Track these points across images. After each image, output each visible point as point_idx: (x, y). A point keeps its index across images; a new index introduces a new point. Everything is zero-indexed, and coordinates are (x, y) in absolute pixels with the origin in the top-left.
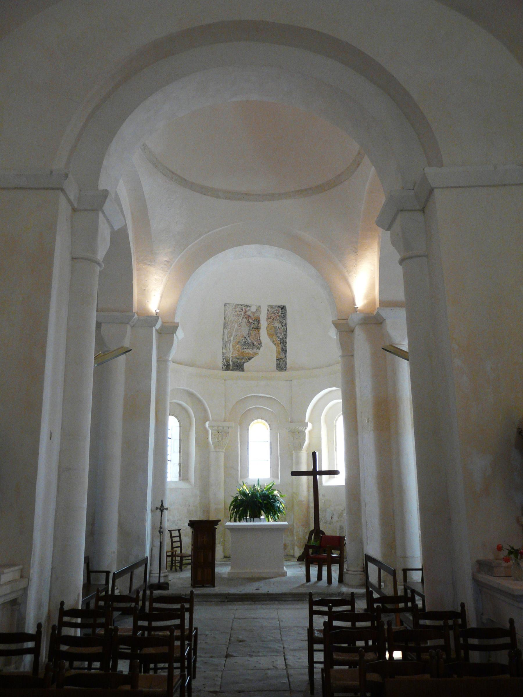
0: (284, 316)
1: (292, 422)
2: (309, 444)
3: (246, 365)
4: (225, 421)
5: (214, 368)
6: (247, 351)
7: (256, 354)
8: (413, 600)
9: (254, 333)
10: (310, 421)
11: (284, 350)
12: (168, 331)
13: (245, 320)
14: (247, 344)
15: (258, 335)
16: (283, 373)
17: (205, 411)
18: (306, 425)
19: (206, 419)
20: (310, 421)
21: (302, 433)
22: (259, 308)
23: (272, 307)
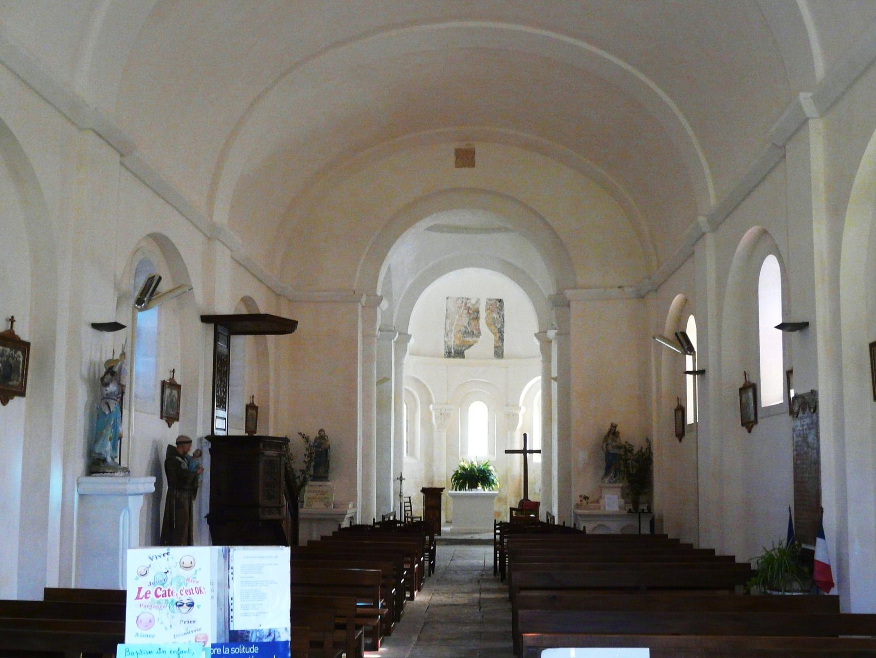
0: (501, 308)
1: (507, 405)
2: (523, 426)
3: (466, 352)
6: (467, 339)
7: (475, 342)
11: (501, 339)
13: (466, 311)
14: (466, 333)
18: (520, 408)
21: (515, 416)
22: (478, 301)
23: (490, 300)
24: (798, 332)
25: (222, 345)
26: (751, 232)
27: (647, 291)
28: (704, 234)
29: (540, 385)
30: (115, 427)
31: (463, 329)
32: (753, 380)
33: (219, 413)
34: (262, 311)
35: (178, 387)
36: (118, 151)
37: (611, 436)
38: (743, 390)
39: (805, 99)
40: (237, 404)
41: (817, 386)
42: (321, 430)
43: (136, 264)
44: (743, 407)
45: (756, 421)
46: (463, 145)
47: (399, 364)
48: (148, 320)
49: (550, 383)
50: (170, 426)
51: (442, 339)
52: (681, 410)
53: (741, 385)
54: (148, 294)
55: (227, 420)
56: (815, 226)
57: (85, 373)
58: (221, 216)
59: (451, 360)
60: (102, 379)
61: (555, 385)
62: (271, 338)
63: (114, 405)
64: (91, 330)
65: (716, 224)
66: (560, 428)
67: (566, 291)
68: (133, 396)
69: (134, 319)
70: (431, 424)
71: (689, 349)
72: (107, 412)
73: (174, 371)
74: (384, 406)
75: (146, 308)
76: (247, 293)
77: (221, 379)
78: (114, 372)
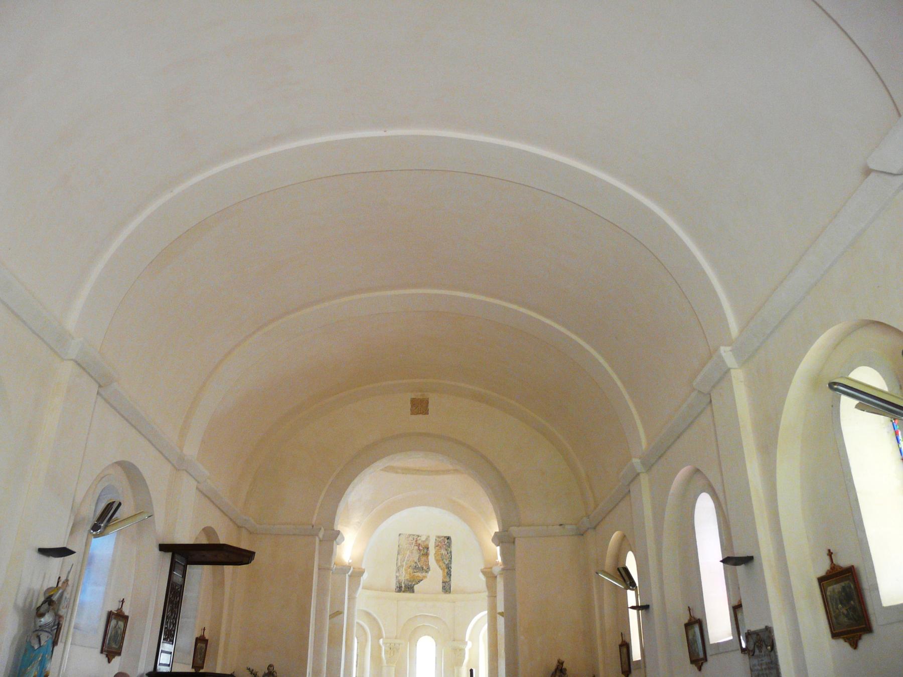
2: (469, 661)
3: (416, 587)
4: (396, 638)
5: (386, 591)
6: (416, 574)
7: (425, 577)
8: (42, 628)
9: (423, 559)
10: (470, 640)
11: (449, 574)
12: (358, 574)
15: (427, 562)
16: (447, 595)
17: (380, 628)
18: (466, 643)
19: (380, 636)
20: (470, 640)
21: (462, 651)
22: (428, 538)
23: (439, 537)
24: (743, 566)
25: (177, 574)
26: (682, 473)
27: (586, 530)
28: (638, 474)
29: (486, 619)
30: (42, 664)
31: (413, 564)
32: (698, 616)
33: (167, 647)
34: (222, 542)
35: (126, 618)
36: (97, 381)
37: (558, 674)
38: (688, 626)
39: (725, 352)
40: (186, 638)
41: (771, 621)
42: (271, 666)
43: (99, 491)
44: (691, 644)
45: (705, 659)
46: (418, 395)
47: (352, 598)
48: (104, 546)
49: (495, 618)
50: (109, 661)
51: (394, 574)
52: (626, 646)
53: (686, 621)
54: (105, 518)
55: (173, 654)
56: (748, 465)
57: (20, 603)
58: (191, 450)
59: (401, 594)
60: (38, 609)
61: (501, 621)
62: (228, 569)
63: (45, 638)
64: (37, 555)
65: (649, 467)
66: (507, 665)
67: (511, 528)
68: (73, 624)
69: (87, 544)
70: (380, 658)
71: (631, 584)
72: (36, 647)
73: (123, 601)
74: (335, 640)
75: (101, 534)
76: (209, 524)
77: (172, 611)
78: (53, 601)
